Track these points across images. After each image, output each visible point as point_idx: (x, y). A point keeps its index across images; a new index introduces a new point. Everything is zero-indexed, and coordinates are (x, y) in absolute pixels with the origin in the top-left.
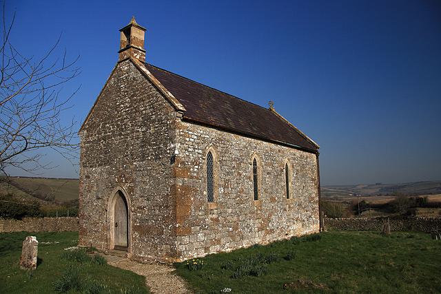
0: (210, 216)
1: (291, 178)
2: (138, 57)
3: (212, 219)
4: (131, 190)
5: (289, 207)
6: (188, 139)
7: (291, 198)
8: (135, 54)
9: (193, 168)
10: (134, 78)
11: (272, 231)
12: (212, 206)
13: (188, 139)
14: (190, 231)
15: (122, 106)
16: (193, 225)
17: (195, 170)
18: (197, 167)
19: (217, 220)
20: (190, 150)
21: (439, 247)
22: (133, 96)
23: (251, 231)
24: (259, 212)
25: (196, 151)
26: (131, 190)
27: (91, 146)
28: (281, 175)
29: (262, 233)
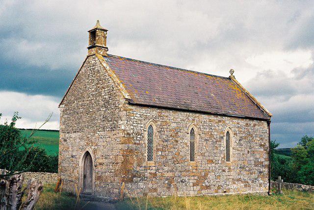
0: (149, 171)
1: (233, 144)
2: (102, 53)
3: (150, 173)
4: (95, 151)
5: (229, 168)
6: (132, 118)
7: (231, 159)
8: (100, 51)
9: (137, 137)
10: (98, 71)
11: (208, 187)
12: (152, 163)
13: (132, 118)
14: (132, 181)
15: (90, 90)
16: (135, 176)
17: (138, 139)
18: (139, 136)
19: (155, 174)
20: (134, 125)
21: (15, 204)
22: (97, 84)
23: (186, 185)
24: (194, 171)
25: (139, 125)
26: (95, 151)
27: (68, 117)
28: (220, 141)
29: (197, 188)
